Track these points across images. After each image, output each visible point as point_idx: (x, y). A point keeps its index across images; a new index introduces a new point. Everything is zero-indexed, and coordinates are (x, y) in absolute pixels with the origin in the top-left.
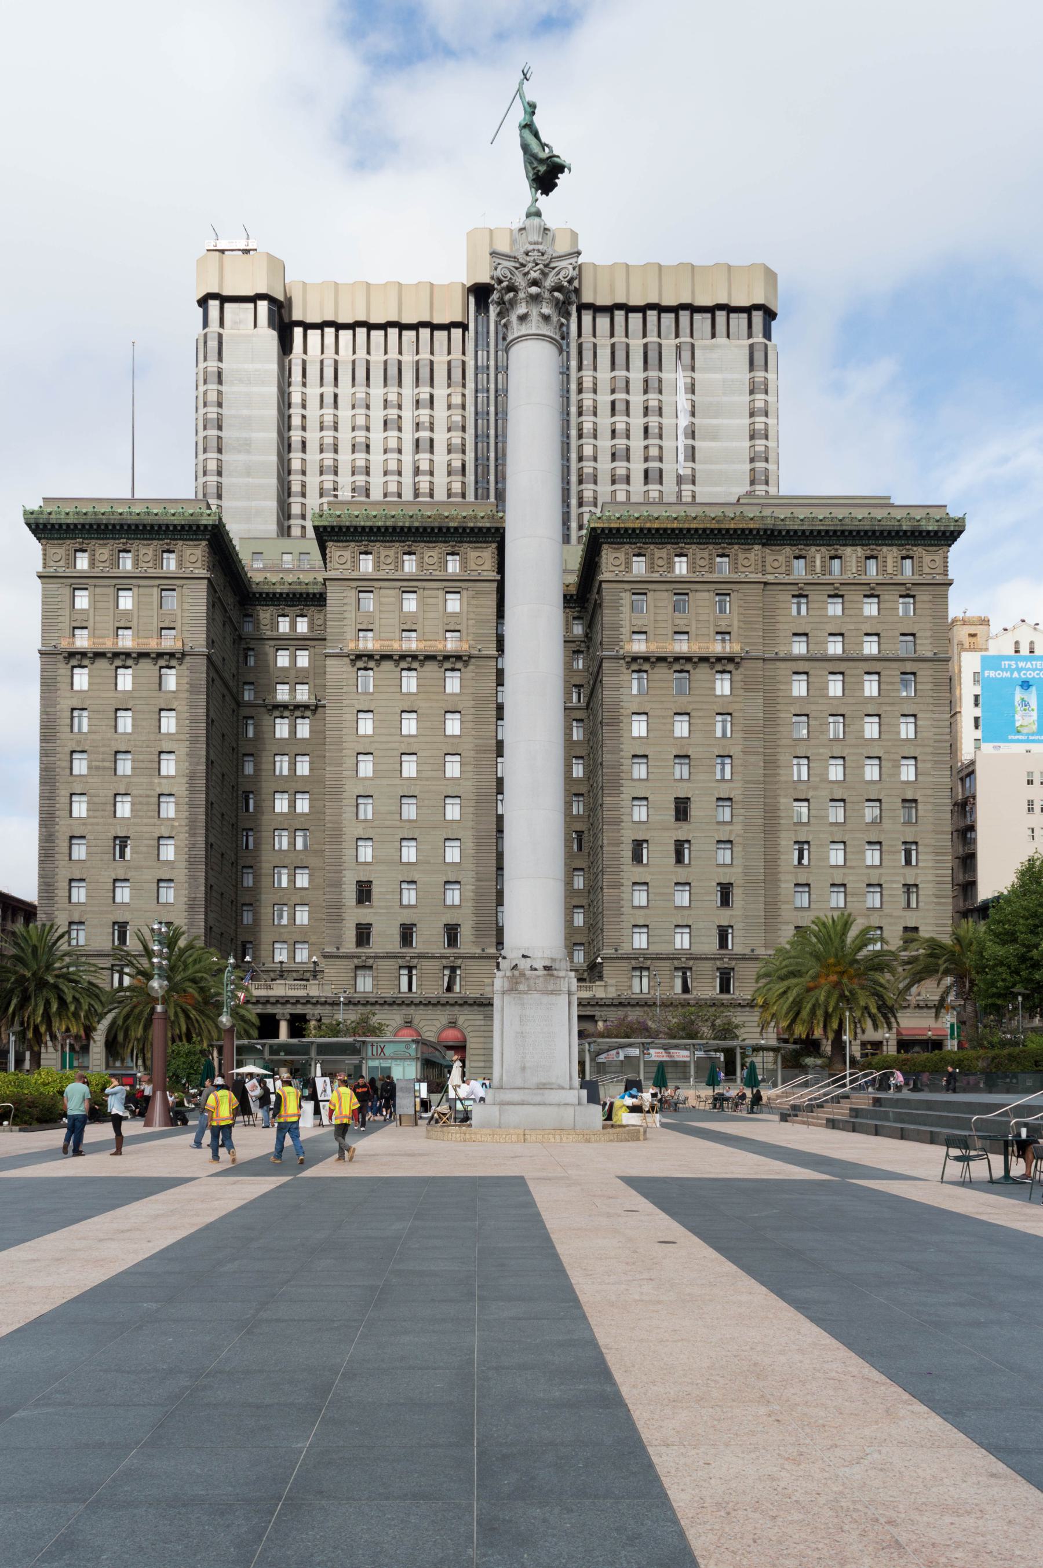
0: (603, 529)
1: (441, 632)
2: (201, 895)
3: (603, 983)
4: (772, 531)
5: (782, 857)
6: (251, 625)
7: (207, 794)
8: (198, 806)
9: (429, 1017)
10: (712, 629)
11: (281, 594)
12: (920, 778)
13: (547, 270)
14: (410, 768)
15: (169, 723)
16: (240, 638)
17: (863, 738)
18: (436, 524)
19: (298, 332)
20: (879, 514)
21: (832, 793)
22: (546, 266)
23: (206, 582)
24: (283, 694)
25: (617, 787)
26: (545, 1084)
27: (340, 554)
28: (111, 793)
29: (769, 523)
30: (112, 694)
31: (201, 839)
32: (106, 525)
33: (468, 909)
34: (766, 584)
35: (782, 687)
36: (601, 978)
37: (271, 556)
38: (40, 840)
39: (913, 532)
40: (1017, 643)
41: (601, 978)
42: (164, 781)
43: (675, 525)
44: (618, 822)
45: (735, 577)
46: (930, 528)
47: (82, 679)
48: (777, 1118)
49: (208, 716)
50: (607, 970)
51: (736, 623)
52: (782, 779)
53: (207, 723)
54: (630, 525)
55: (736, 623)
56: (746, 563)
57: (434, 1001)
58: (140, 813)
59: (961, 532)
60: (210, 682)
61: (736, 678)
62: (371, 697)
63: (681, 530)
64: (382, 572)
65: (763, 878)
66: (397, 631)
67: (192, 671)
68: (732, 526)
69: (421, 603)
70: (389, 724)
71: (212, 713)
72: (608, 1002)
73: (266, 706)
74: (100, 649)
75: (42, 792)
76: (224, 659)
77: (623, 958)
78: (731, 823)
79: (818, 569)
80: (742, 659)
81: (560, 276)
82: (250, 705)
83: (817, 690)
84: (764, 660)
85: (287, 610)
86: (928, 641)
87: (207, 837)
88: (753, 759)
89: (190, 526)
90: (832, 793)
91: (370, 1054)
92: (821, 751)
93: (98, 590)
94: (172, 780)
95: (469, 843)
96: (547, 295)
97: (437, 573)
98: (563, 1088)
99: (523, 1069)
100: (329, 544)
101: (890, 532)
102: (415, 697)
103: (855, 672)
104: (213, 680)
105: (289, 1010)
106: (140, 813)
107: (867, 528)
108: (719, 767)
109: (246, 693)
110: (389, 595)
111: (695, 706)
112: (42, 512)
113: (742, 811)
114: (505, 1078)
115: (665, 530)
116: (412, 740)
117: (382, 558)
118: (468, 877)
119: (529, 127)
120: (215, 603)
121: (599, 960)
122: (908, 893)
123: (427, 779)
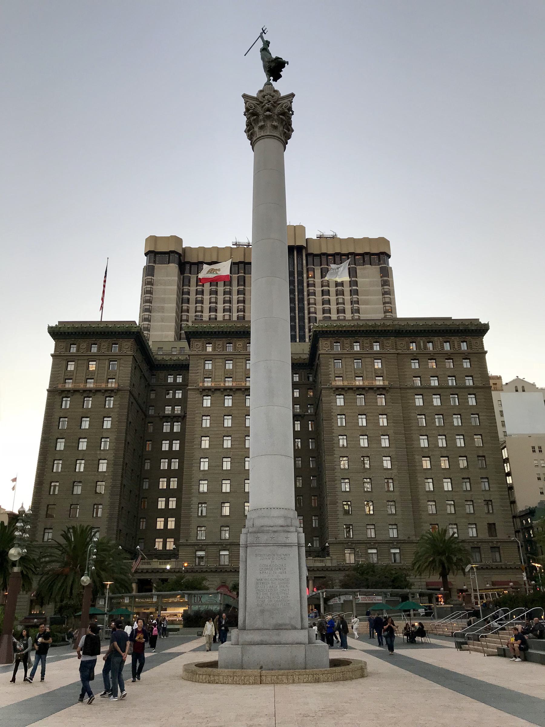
0: (319, 331)
1: (244, 378)
2: (116, 512)
3: (329, 558)
4: (399, 330)
5: (420, 486)
6: (154, 379)
7: (124, 459)
10: (374, 374)
11: (170, 365)
12: (484, 445)
13: (275, 105)
16: (149, 385)
18: (242, 330)
19: (188, 267)
20: (448, 323)
22: (275, 102)
23: (132, 357)
25: (332, 452)
26: (281, 625)
27: (197, 344)
28: (74, 460)
29: (397, 327)
30: (81, 410)
32: (86, 333)
34: (398, 354)
36: (328, 555)
37: (162, 335)
39: (465, 330)
40: (516, 387)
41: (328, 555)
42: (102, 452)
43: (353, 329)
45: (383, 351)
46: (473, 328)
47: (67, 403)
48: (453, 645)
49: (127, 420)
50: (331, 550)
51: (385, 372)
53: (127, 423)
54: (332, 329)
55: (385, 372)
56: (387, 345)
57: (214, 570)
60: (131, 404)
63: (356, 331)
65: (410, 498)
68: (380, 329)
70: (218, 421)
71: (130, 420)
72: (333, 569)
73: (159, 417)
74: (77, 388)
76: (139, 394)
79: (422, 347)
80: (389, 388)
81: (283, 107)
82: (152, 416)
85: (172, 372)
86: (479, 379)
87: (122, 481)
89: (126, 332)
91: (193, 602)
92: (434, 432)
93: (80, 362)
94: (107, 452)
96: (276, 117)
97: (242, 351)
98: (295, 628)
100: (192, 340)
101: (454, 330)
102: (230, 409)
104: (132, 403)
105: (158, 576)
107: (443, 329)
109: (150, 411)
110: (219, 362)
114: (247, 622)
115: (348, 331)
116: (229, 429)
117: (217, 345)
119: (265, 49)
120: (136, 367)
121: (327, 544)
122: (487, 504)
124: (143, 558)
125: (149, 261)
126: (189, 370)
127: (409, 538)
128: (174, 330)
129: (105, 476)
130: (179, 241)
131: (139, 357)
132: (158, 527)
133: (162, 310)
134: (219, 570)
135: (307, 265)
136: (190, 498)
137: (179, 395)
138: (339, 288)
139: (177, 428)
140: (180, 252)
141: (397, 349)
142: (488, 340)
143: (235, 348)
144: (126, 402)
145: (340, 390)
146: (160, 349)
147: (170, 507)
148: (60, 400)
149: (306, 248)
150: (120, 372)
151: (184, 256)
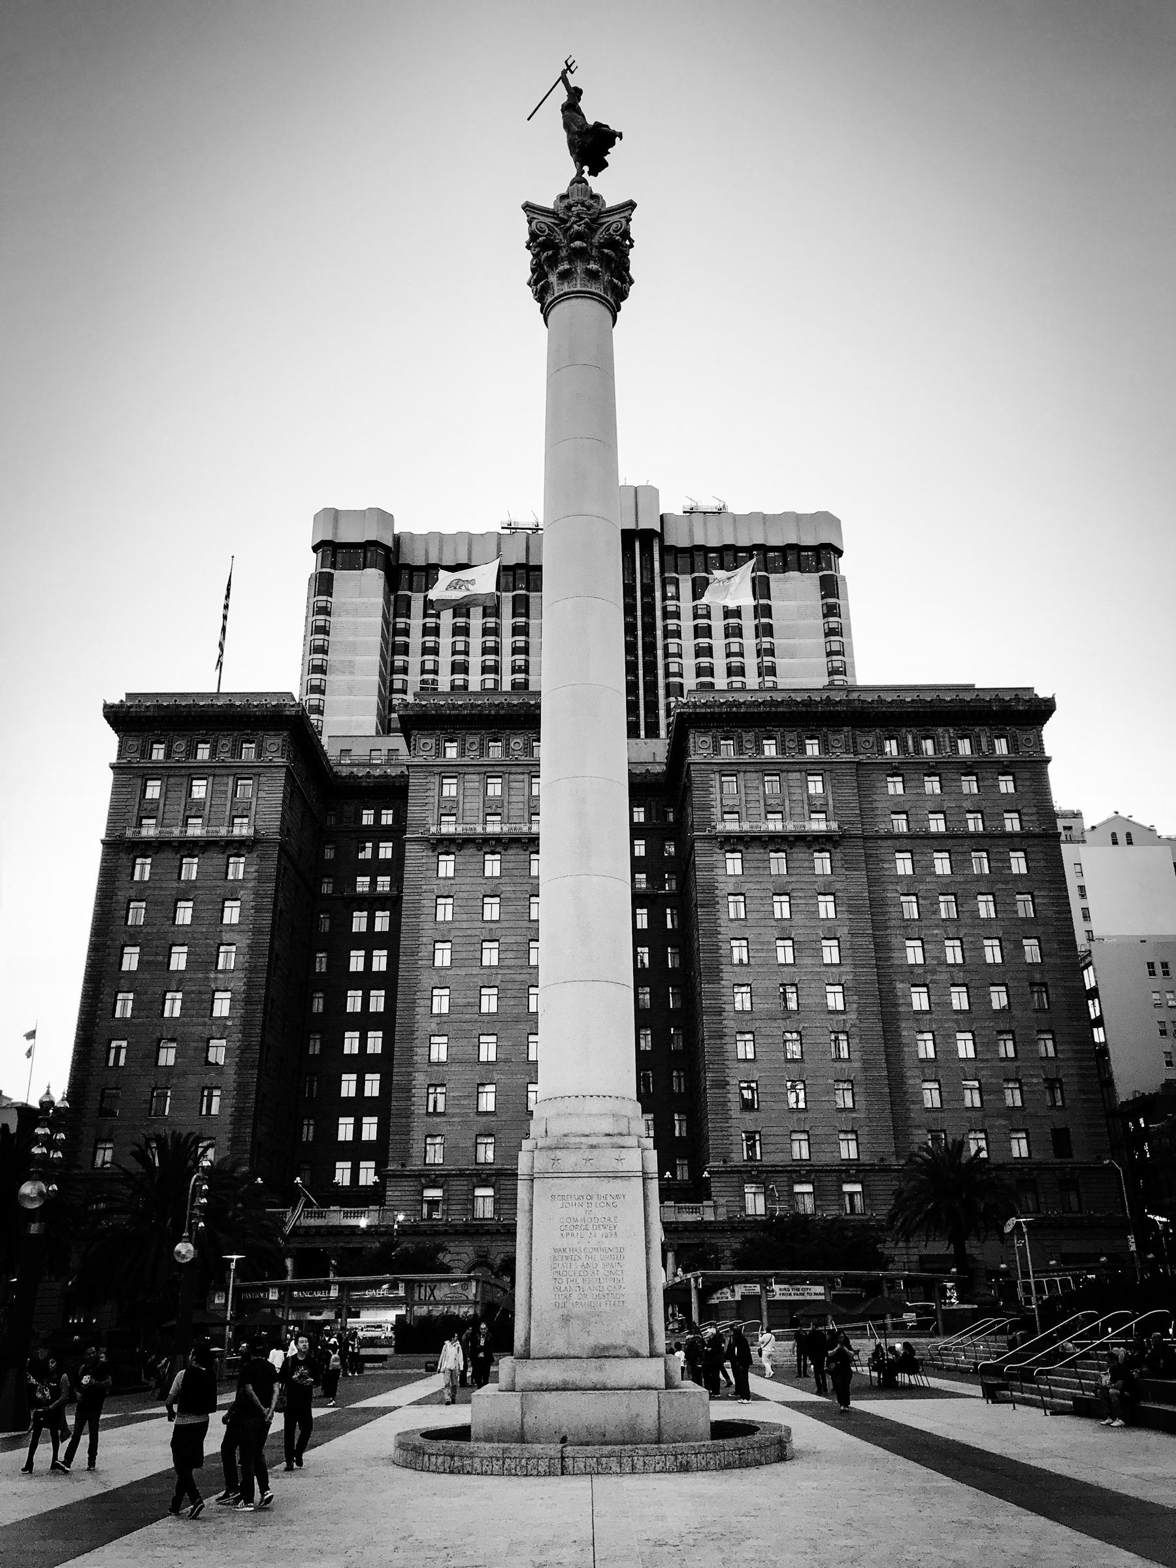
3: (711, 1203)
5: (906, 1049)
8: (257, 1003)
10: (806, 807)
14: (491, 956)
15: (441, 1004)
17: (978, 917)
21: (952, 978)
25: (715, 974)
26: (606, 1348)
35: (886, 866)
37: (350, 723)
44: (720, 1012)
50: (715, 1186)
51: (831, 802)
52: (896, 962)
55: (831, 802)
56: (835, 744)
58: (191, 1012)
61: (838, 856)
62: (452, 882)
64: (466, 758)
66: (481, 814)
69: (507, 788)
70: (470, 908)
77: (732, 1172)
78: (843, 1012)
79: (911, 749)
83: (923, 869)
84: (865, 838)
87: (263, 1036)
88: (861, 941)
90: (952, 978)
91: (416, 1298)
92: (935, 932)
97: (523, 758)
98: (637, 1355)
99: (566, 1319)
102: (497, 881)
103: (960, 849)
106: (191, 1012)
111: (794, 886)
113: (856, 998)
114: (533, 1341)
120: (293, 795)
121: (706, 1174)
123: (509, 967)
127: (882, 1160)
129: (226, 1027)
130: (386, 519)
133: (350, 667)
134: (472, 1230)
135: (662, 571)
136: (410, 1074)
139: (386, 851)
140: (389, 543)
141: (856, 753)
142: (1052, 734)
143: (507, 751)
144: (271, 866)
145: (733, 842)
146: (345, 752)
149: (661, 536)
150: (258, 804)
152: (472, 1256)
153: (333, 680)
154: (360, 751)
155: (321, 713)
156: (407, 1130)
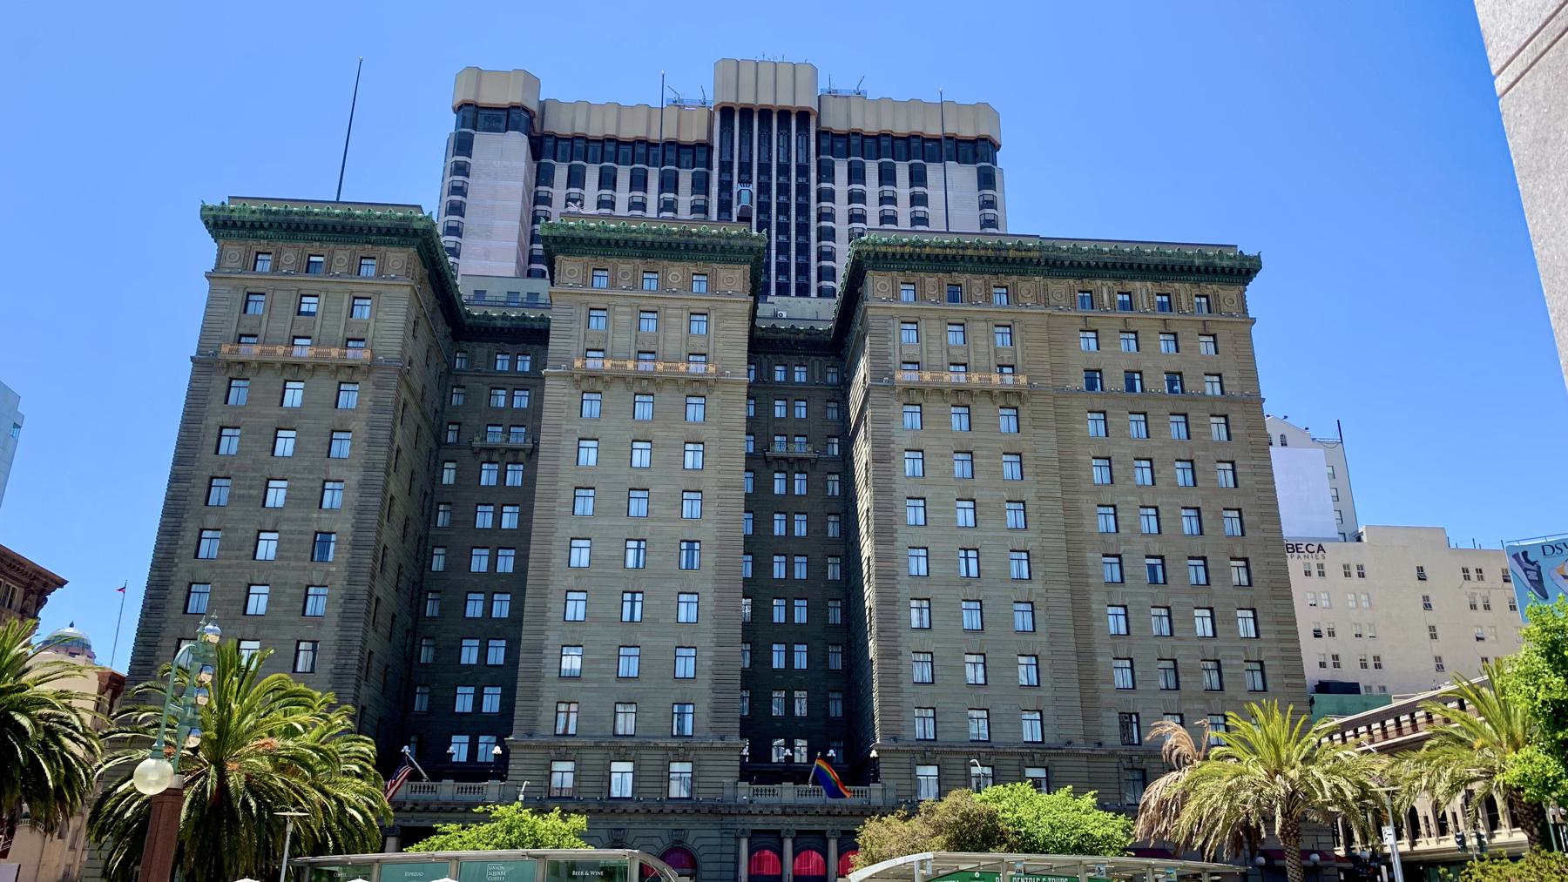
2: (354, 661)
3: (879, 786)
5: (1096, 624)
7: (379, 533)
9: (647, 833)
11: (502, 329)
21: (1147, 548)
23: (408, 289)
24: (495, 436)
31: (362, 590)
33: (705, 681)
37: (488, 262)
38: (149, 586)
42: (324, 515)
49: (392, 440)
50: (884, 769)
59: (1256, 271)
67: (378, 386)
71: (398, 440)
75: (163, 524)
90: (1147, 548)
95: (709, 599)
100: (559, 258)
108: (963, 561)
112: (223, 209)
118: (706, 640)
121: (874, 754)
124: (414, 776)
125: (462, 122)
126: (547, 343)
128: (518, 217)
129: (328, 573)
130: (532, 82)
131: (429, 295)
132: (458, 709)
135: (818, 154)
136: (541, 632)
137: (521, 401)
138: (886, 207)
139: (521, 401)
140: (534, 107)
144: (389, 397)
146: (480, 294)
147: (491, 661)
148: (225, 386)
150: (379, 312)
151: (543, 114)
152: (667, 841)
153: (474, 183)
154: (496, 292)
155: (457, 256)
156: (535, 695)
